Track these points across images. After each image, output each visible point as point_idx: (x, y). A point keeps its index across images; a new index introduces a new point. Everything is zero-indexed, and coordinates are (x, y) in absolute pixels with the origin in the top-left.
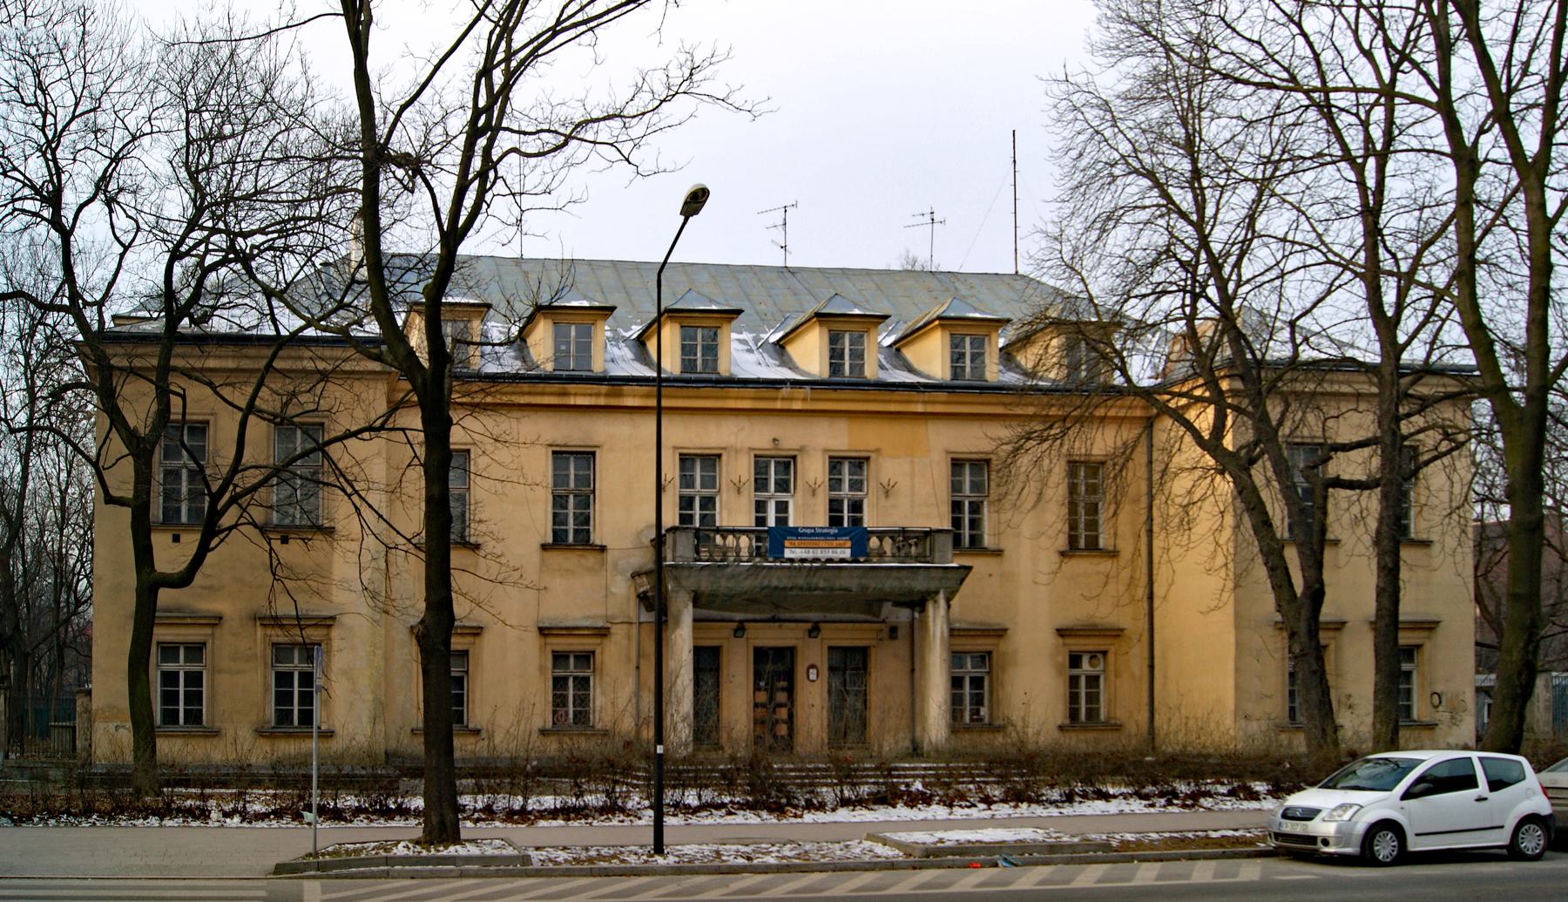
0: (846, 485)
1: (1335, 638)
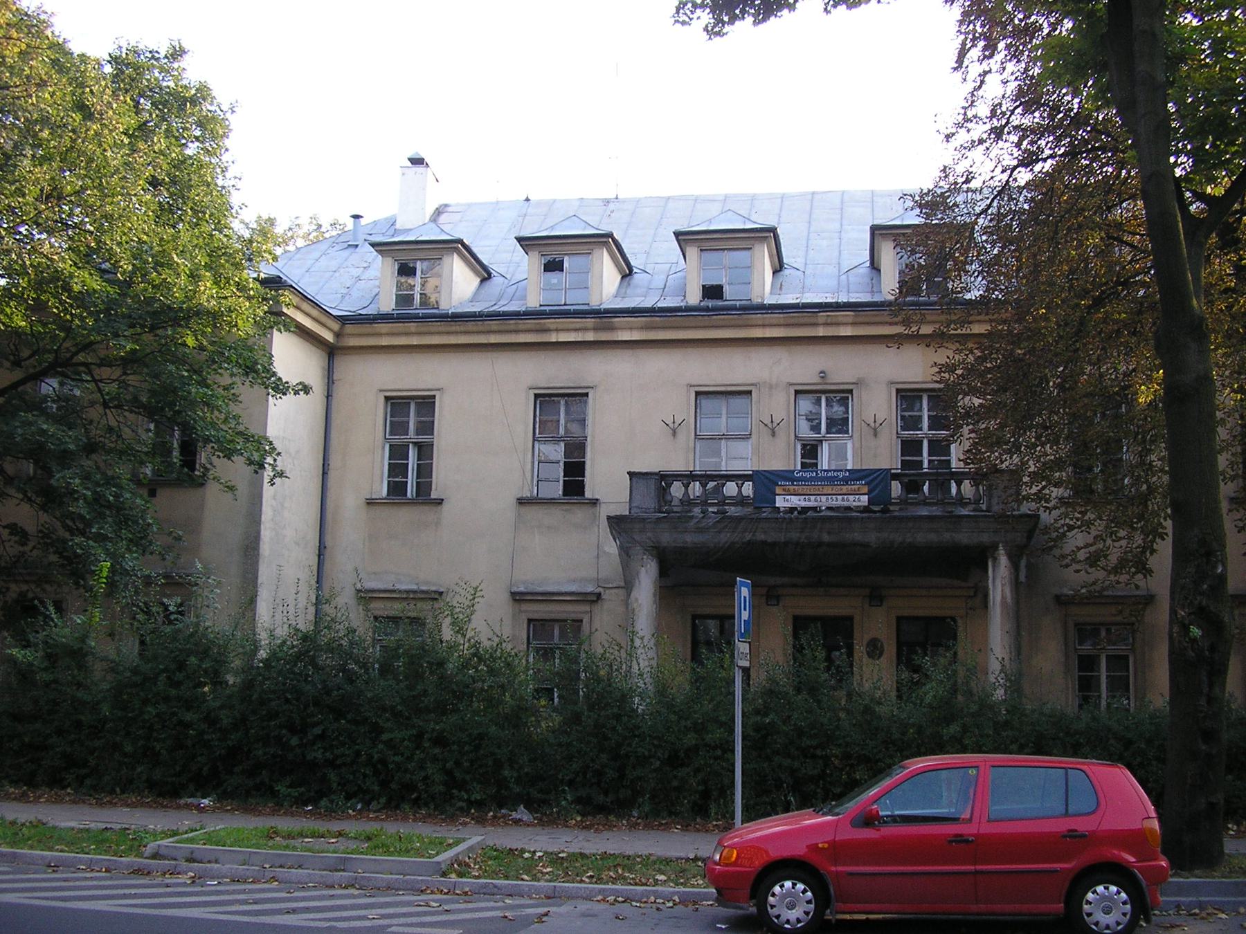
0: (925, 423)
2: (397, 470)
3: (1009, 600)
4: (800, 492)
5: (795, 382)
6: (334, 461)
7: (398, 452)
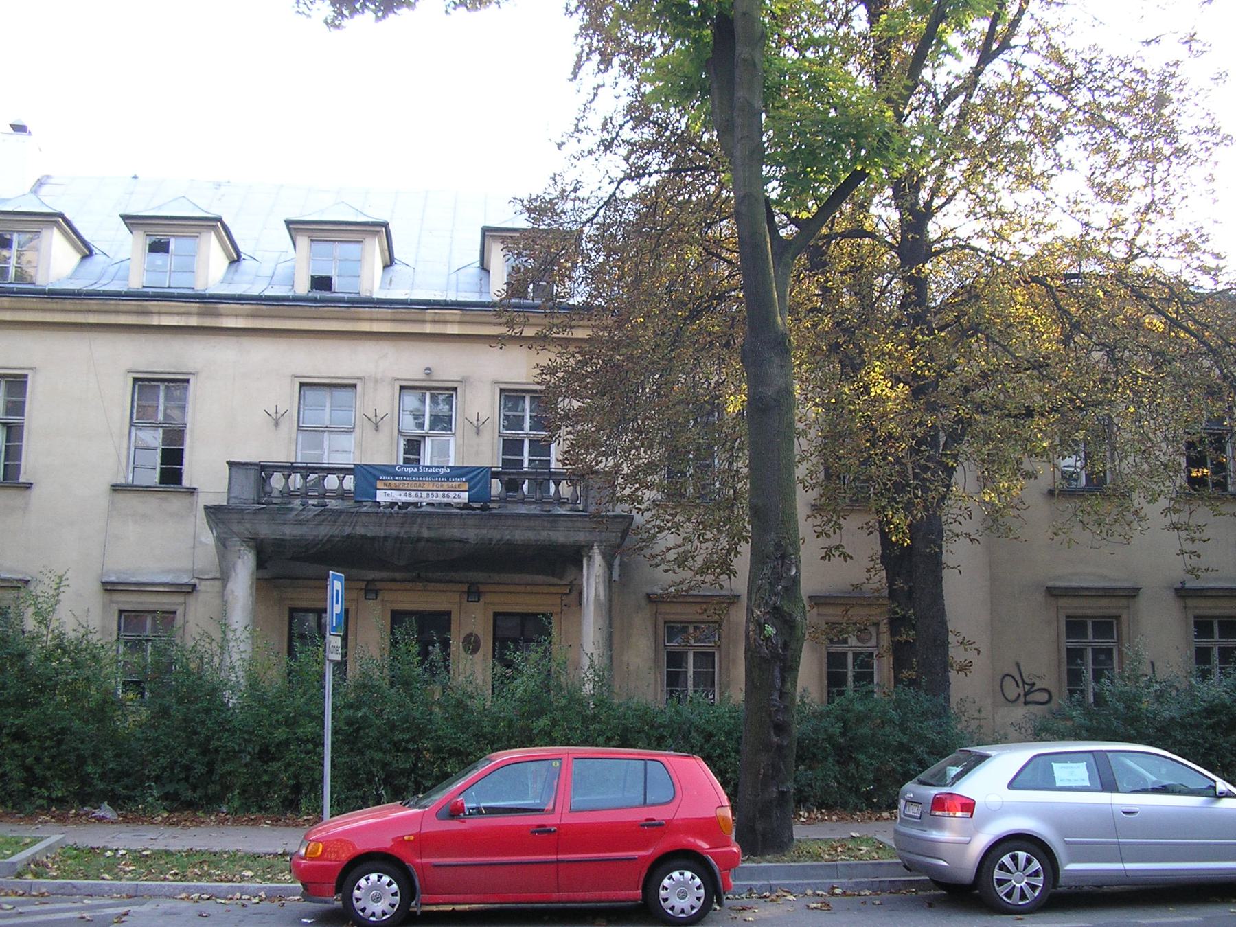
0: (527, 423)
1: (1128, 607)
3: (602, 597)
4: (401, 487)
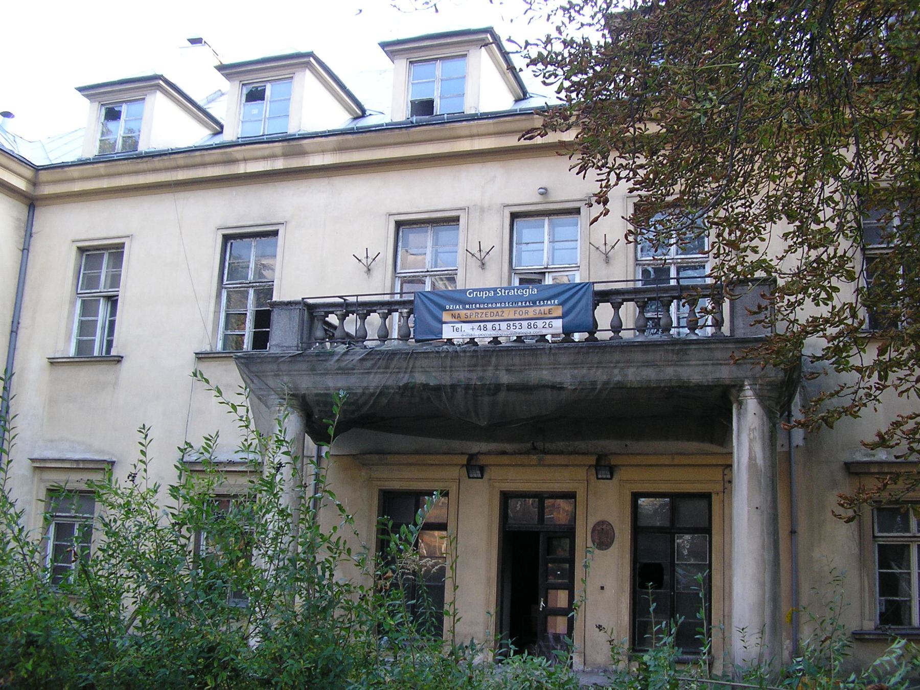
2: (86, 328)
3: (760, 461)
4: (473, 318)
5: (510, 203)
6: (25, 321)
7: (88, 307)
